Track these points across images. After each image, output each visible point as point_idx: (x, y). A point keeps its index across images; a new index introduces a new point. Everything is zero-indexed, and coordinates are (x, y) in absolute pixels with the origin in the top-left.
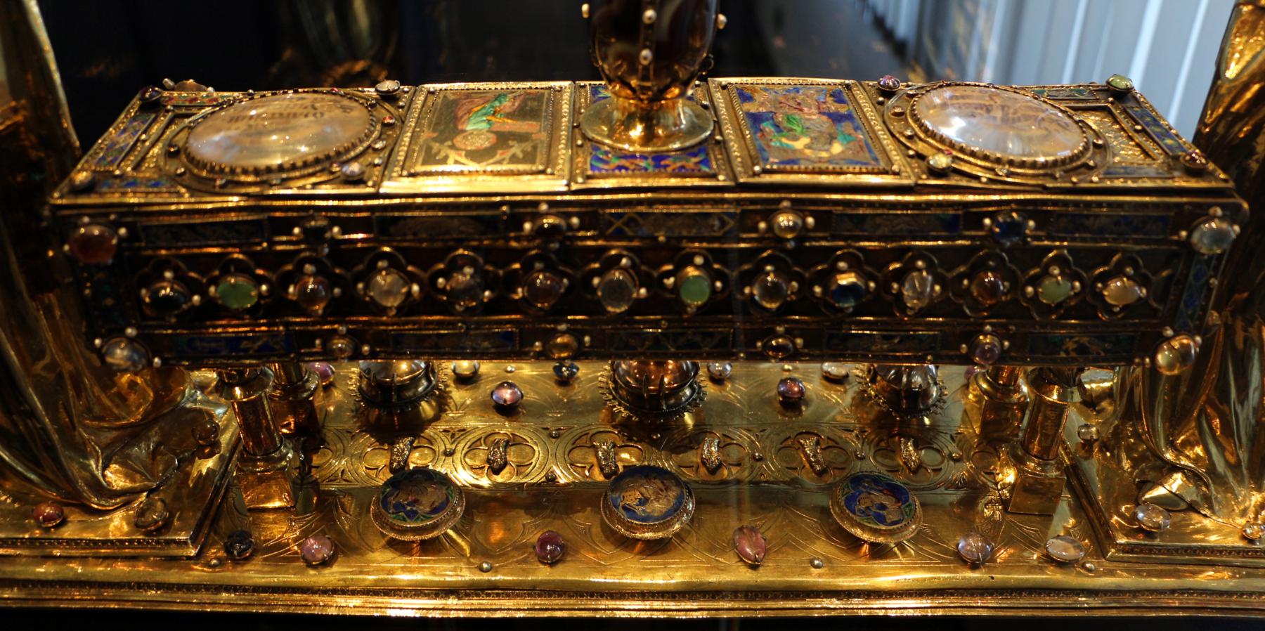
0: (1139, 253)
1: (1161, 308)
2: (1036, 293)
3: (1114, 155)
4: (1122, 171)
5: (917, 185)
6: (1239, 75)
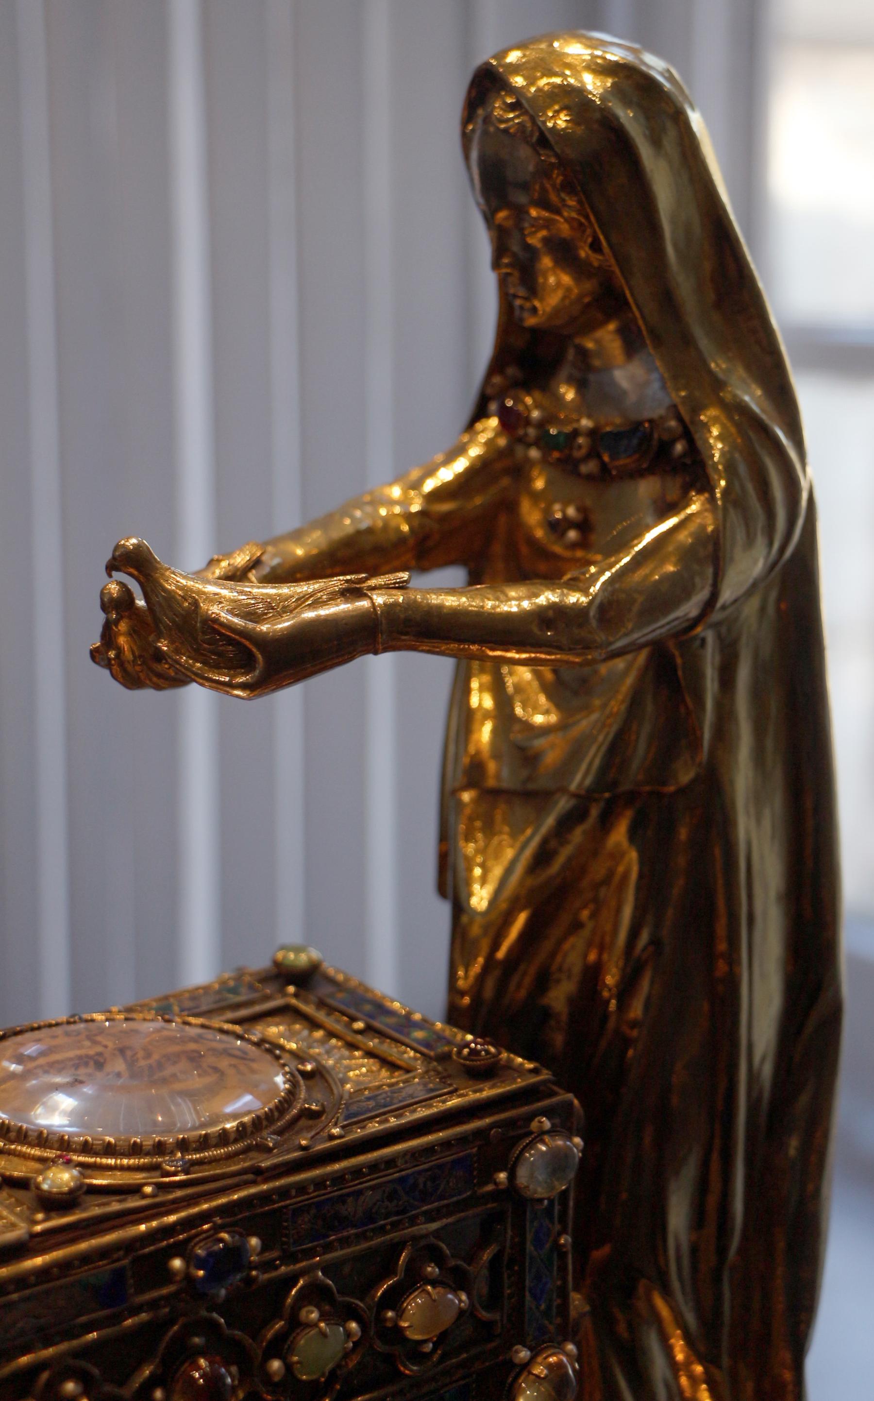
0: (437, 1233)
1: (496, 1316)
2: (288, 1367)
3: (344, 1081)
4: (372, 1104)
5: (33, 1236)
6: (493, 902)
